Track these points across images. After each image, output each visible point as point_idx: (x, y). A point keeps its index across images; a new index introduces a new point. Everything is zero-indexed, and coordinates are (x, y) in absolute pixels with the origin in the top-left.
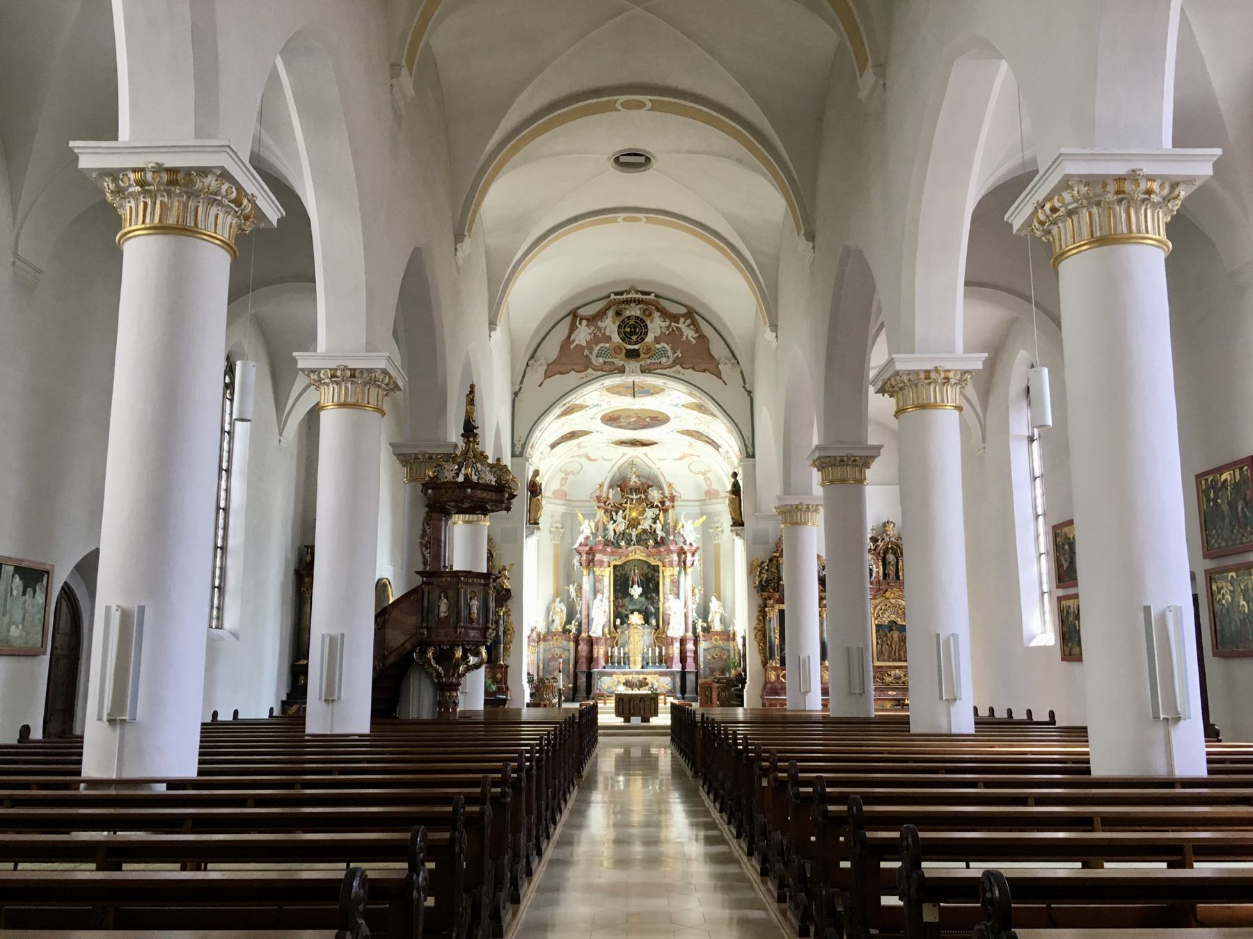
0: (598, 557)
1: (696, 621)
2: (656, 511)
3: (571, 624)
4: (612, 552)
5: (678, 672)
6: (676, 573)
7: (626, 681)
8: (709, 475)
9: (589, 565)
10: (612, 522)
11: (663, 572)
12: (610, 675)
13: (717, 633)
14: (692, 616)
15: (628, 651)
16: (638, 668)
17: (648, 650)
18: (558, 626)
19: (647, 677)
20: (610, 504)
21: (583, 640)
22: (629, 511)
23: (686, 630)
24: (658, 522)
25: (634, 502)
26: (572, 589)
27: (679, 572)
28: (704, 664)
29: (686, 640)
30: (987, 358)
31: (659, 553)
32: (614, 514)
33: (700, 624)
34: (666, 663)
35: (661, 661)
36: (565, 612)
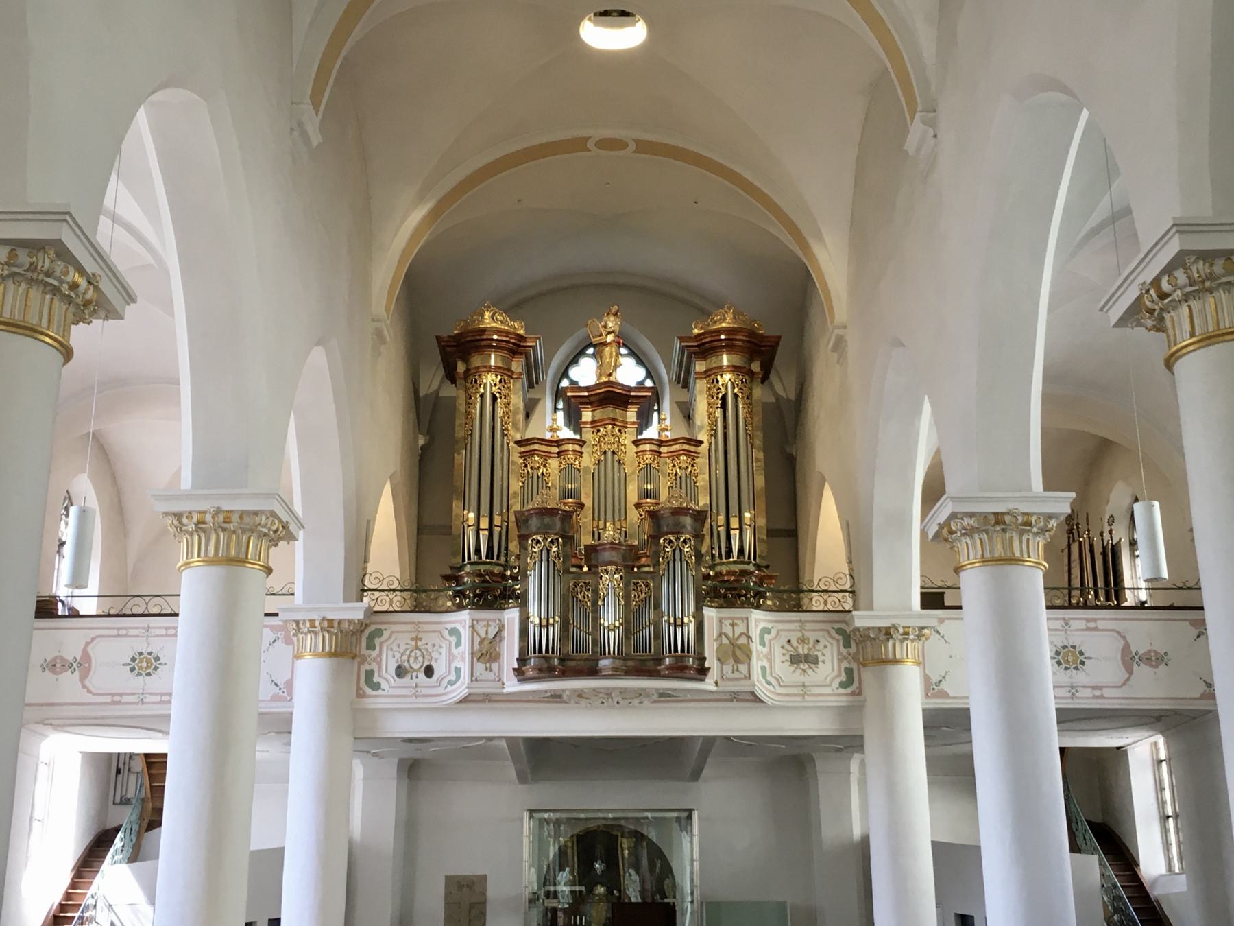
30: (1075, 500)
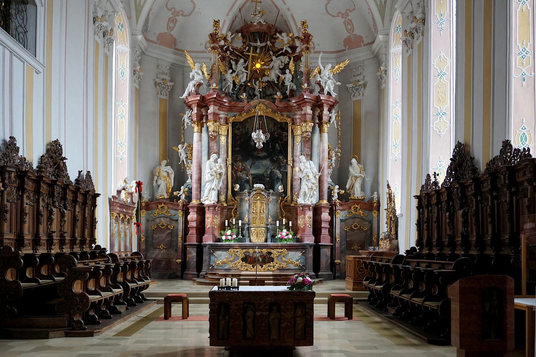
2: (285, 59)
3: (180, 190)
5: (311, 246)
7: (246, 256)
8: (351, 16)
10: (231, 71)
11: (292, 131)
13: (358, 201)
14: (327, 180)
18: (162, 193)
20: (227, 49)
21: (193, 207)
23: (321, 197)
24: (287, 71)
25: (258, 51)
27: (314, 128)
32: (233, 63)
36: (172, 176)
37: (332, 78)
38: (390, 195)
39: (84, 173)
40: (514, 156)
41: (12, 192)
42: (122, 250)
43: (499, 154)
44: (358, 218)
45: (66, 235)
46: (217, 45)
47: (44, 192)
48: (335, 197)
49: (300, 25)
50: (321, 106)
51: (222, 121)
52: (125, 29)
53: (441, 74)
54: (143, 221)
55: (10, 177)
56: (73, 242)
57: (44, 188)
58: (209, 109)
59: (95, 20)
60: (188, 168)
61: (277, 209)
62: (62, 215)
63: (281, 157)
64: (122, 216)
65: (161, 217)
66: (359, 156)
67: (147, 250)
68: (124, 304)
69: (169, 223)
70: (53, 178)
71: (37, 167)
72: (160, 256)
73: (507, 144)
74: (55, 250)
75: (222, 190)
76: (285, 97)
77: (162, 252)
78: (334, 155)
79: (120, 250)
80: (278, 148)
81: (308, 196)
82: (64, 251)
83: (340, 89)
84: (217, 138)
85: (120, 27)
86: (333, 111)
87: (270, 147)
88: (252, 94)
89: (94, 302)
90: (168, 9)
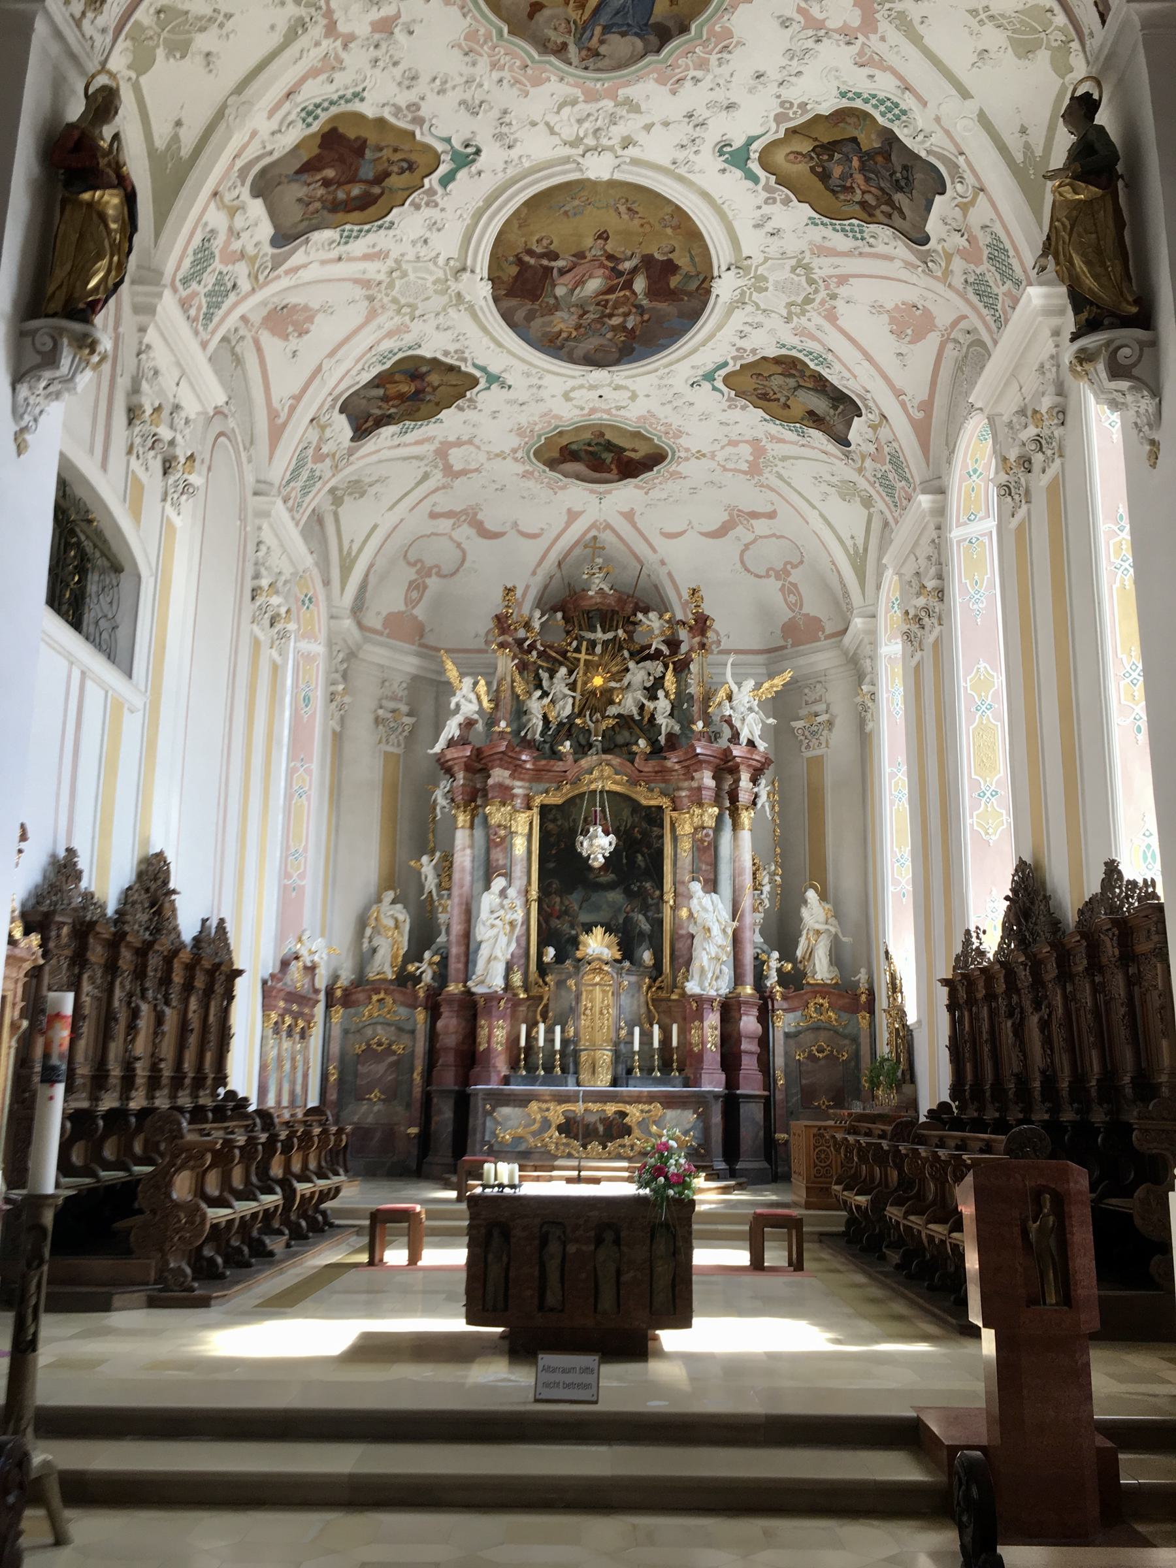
0: (499, 775)
1: (764, 957)
2: (656, 667)
3: (421, 960)
4: (538, 770)
5: (716, 1096)
6: (710, 822)
8: (795, 576)
9: (474, 800)
10: (539, 693)
12: (522, 1101)
13: (822, 989)
14: (753, 940)
15: (576, 1034)
16: (602, 1082)
17: (631, 1033)
18: (384, 965)
19: (628, 1109)
20: (532, 647)
21: (451, 1000)
22: (585, 674)
23: (738, 979)
24: (661, 694)
25: (598, 649)
26: (427, 867)
27: (719, 819)
28: (787, 1075)
29: (739, 1004)
31: (663, 773)
32: (545, 676)
33: (774, 961)
34: (680, 1070)
35: (666, 1066)
37: (757, 709)
38: (893, 977)
39: (214, 923)
40: (1127, 897)
41: (60, 967)
42: (285, 1103)
43: (1099, 891)
44: (825, 1029)
45: (162, 1065)
46: (510, 640)
47: (125, 968)
48: (772, 979)
49: (686, 595)
50: (734, 771)
51: (518, 802)
52: (317, 605)
53: (984, 708)
54: (336, 1032)
55: (58, 936)
56: (177, 1082)
57: (126, 958)
58: (489, 776)
59: (255, 593)
60: (440, 909)
61: (639, 1006)
62: (159, 1020)
63: (648, 885)
64: (288, 1020)
65: (376, 1023)
66: (824, 884)
67: (340, 1105)
68: (282, 1233)
69: (393, 1038)
70: (147, 936)
71: (117, 912)
72: (370, 1119)
73: (1112, 869)
74: (137, 1103)
75: (515, 960)
76: (657, 751)
77: (376, 1108)
78: (766, 880)
79: (279, 1102)
80: (642, 864)
81: (710, 975)
82: (157, 1103)
83: (779, 734)
84: (508, 838)
85: (307, 602)
86: (763, 782)
87: (624, 861)
88: (583, 742)
89: (217, 1225)
90: (409, 563)
